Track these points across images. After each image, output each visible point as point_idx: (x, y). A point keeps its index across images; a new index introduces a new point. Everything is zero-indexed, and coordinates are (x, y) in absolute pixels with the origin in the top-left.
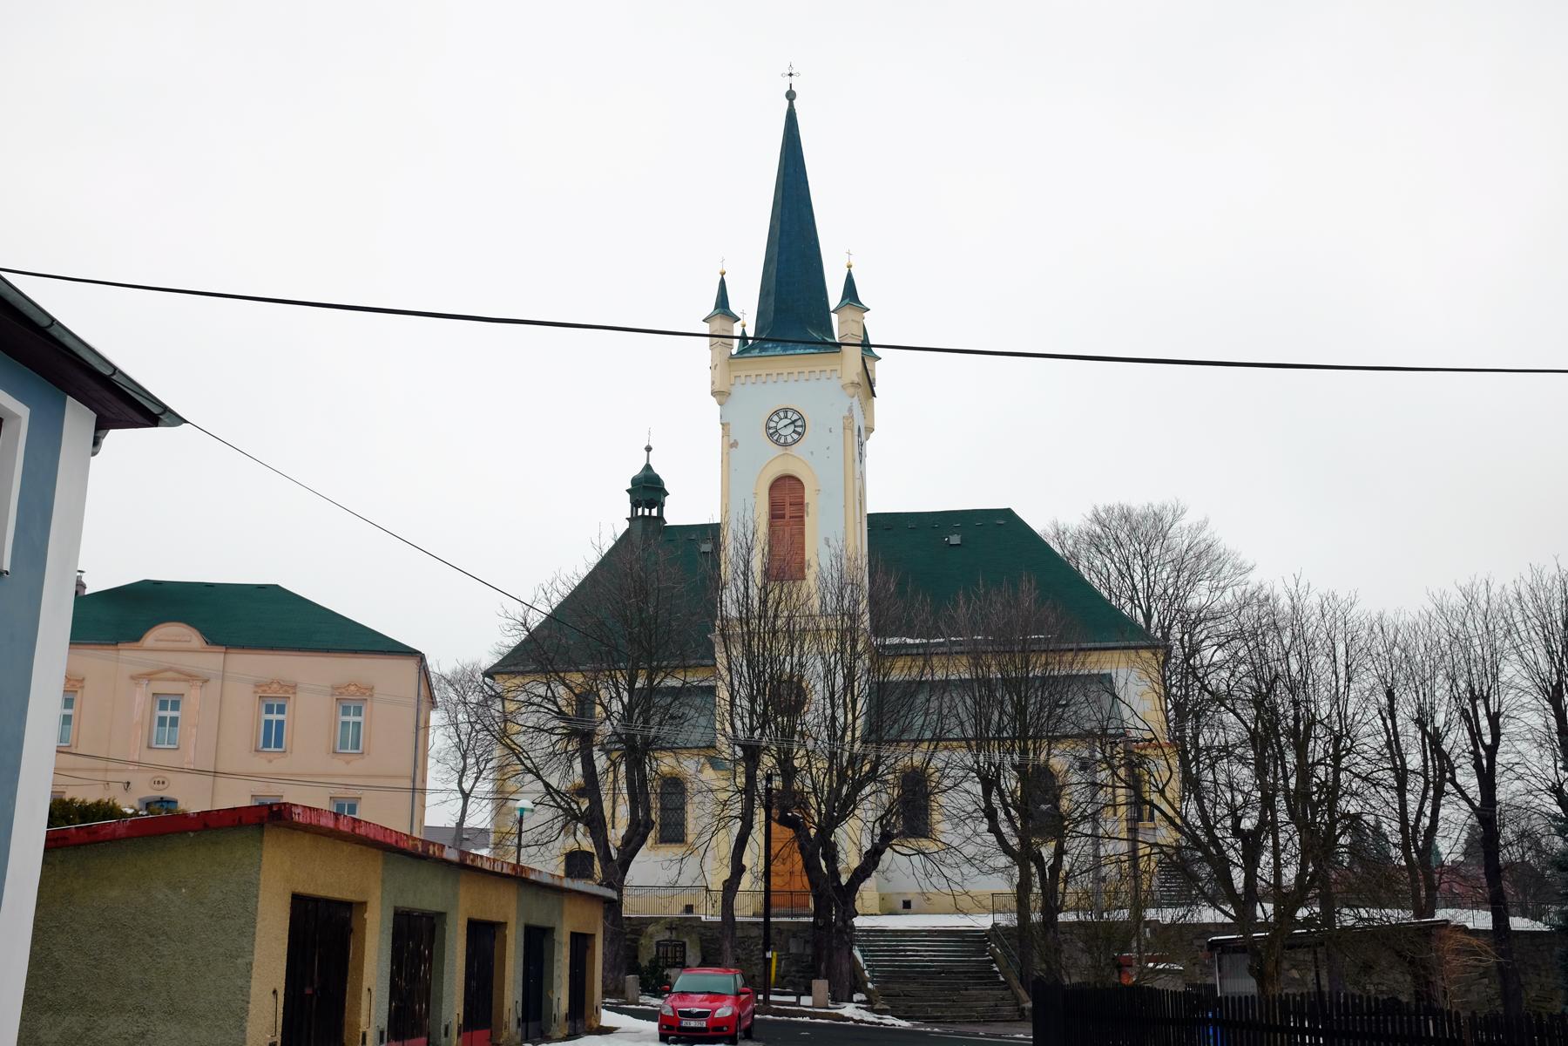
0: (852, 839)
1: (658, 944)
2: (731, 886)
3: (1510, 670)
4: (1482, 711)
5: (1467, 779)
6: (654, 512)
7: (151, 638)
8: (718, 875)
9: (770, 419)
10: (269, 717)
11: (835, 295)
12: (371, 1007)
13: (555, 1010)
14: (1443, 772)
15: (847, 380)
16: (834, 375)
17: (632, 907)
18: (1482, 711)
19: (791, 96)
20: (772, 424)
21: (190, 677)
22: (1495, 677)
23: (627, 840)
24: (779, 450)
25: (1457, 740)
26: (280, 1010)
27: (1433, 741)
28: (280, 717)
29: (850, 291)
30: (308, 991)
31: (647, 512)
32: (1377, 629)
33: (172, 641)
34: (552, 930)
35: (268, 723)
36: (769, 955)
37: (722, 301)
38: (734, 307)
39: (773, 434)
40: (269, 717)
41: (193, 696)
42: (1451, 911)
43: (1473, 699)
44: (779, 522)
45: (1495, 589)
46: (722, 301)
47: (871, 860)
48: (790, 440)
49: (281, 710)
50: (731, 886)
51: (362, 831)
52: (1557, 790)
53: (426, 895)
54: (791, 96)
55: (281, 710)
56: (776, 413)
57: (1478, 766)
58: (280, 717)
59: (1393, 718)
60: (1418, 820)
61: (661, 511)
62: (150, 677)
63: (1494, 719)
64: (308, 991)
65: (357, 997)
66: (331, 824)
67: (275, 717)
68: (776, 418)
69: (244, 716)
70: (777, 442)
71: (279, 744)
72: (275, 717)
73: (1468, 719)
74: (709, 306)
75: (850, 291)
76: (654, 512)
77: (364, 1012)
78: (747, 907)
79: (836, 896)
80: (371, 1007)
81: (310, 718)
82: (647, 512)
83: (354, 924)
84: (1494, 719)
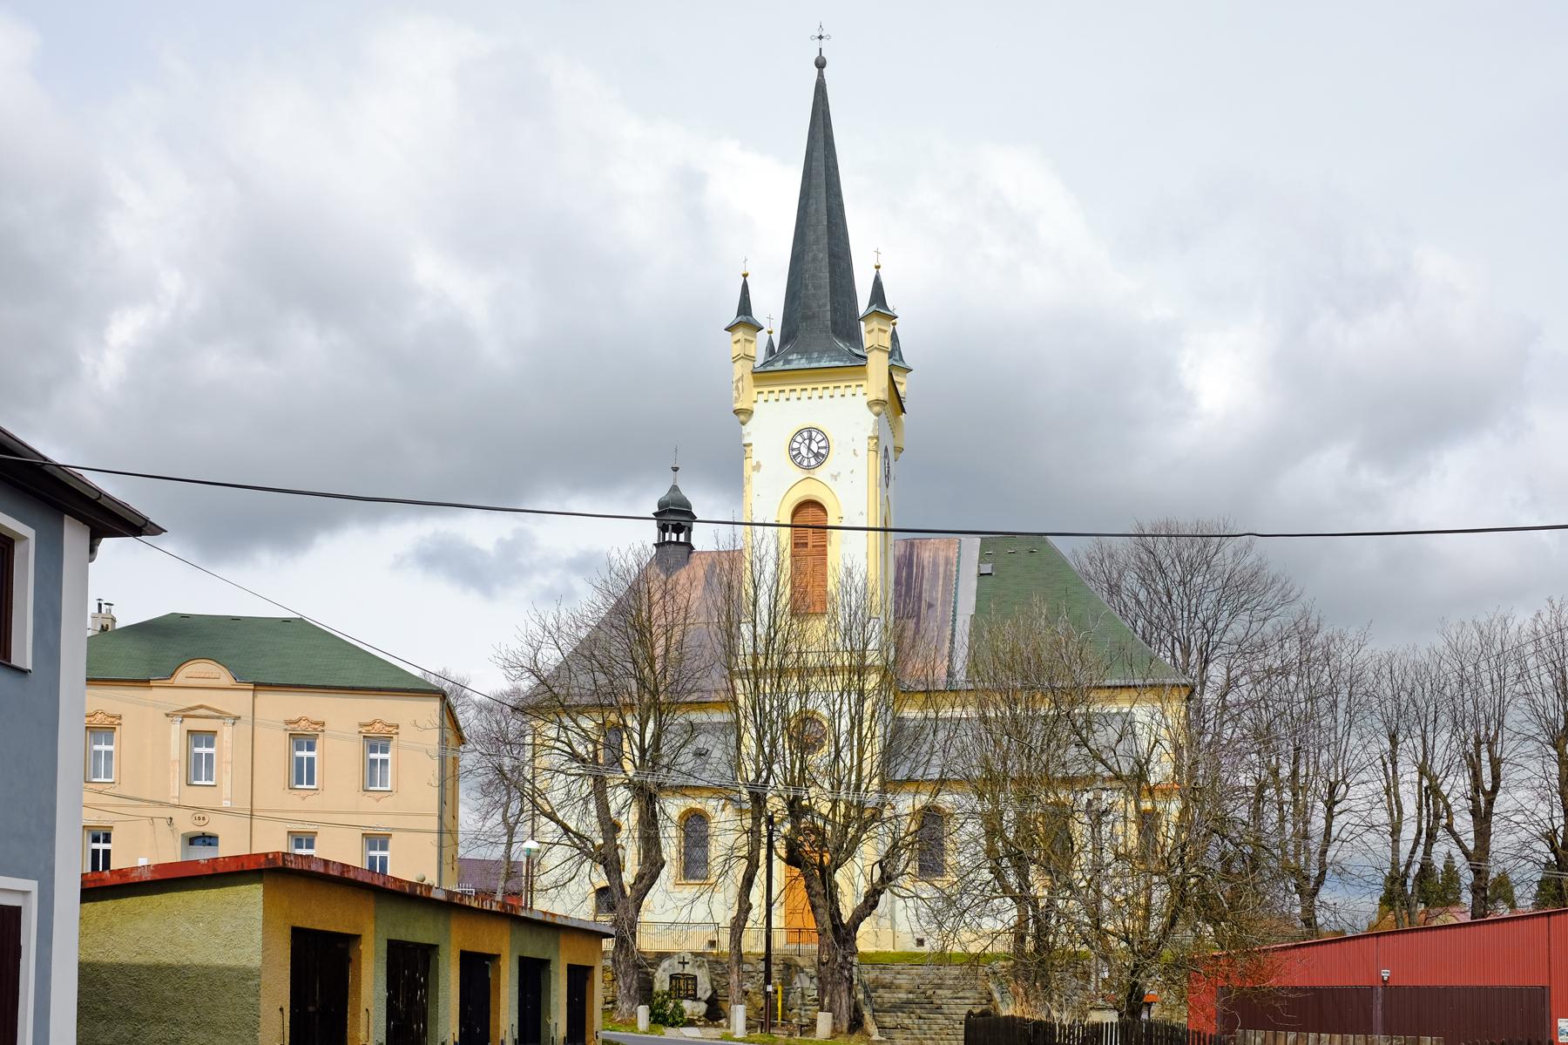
0: (851, 882)
1: (672, 977)
2: (738, 926)
3: (1516, 717)
4: (1485, 756)
5: (1464, 824)
6: (682, 538)
7: (181, 677)
8: (724, 913)
9: (793, 440)
10: (95, 846)
11: (863, 304)
12: (558, 1021)
13: (553, 1033)
14: (1437, 817)
15: (873, 397)
16: (860, 391)
17: (647, 942)
18: (1485, 756)
19: (820, 64)
20: (795, 445)
21: (220, 715)
22: (1500, 724)
23: (640, 877)
24: (800, 474)
25: (1456, 786)
26: (287, 1024)
27: (1431, 792)
28: (107, 846)
29: (878, 294)
30: (311, 1009)
31: (674, 537)
32: (1385, 671)
33: (203, 679)
34: (547, 962)
35: (95, 853)
36: (770, 988)
37: (745, 306)
38: (758, 314)
39: (795, 456)
40: (95, 846)
41: (226, 733)
42: (264, 1005)
43: (1478, 743)
44: (803, 551)
45: (1513, 629)
46: (745, 306)
47: (870, 904)
48: (819, 438)
49: (107, 840)
50: (738, 926)
51: (351, 875)
52: (1550, 837)
53: (419, 931)
54: (820, 64)
55: (107, 840)
57: (1474, 813)
58: (107, 846)
59: (1394, 764)
60: (1408, 866)
61: (688, 537)
62: (185, 714)
63: (1496, 763)
64: (311, 1009)
65: (357, 1015)
66: (321, 870)
67: (101, 846)
68: (799, 439)
69: (275, 752)
70: (800, 465)
71: (311, 781)
72: (101, 846)
73: (1474, 768)
74: (731, 315)
75: (878, 294)
76: (682, 538)
77: (363, 1028)
78: (753, 943)
79: (843, 934)
80: (558, 1021)
81: (338, 757)
82: (674, 536)
83: (352, 955)
84: (1496, 763)
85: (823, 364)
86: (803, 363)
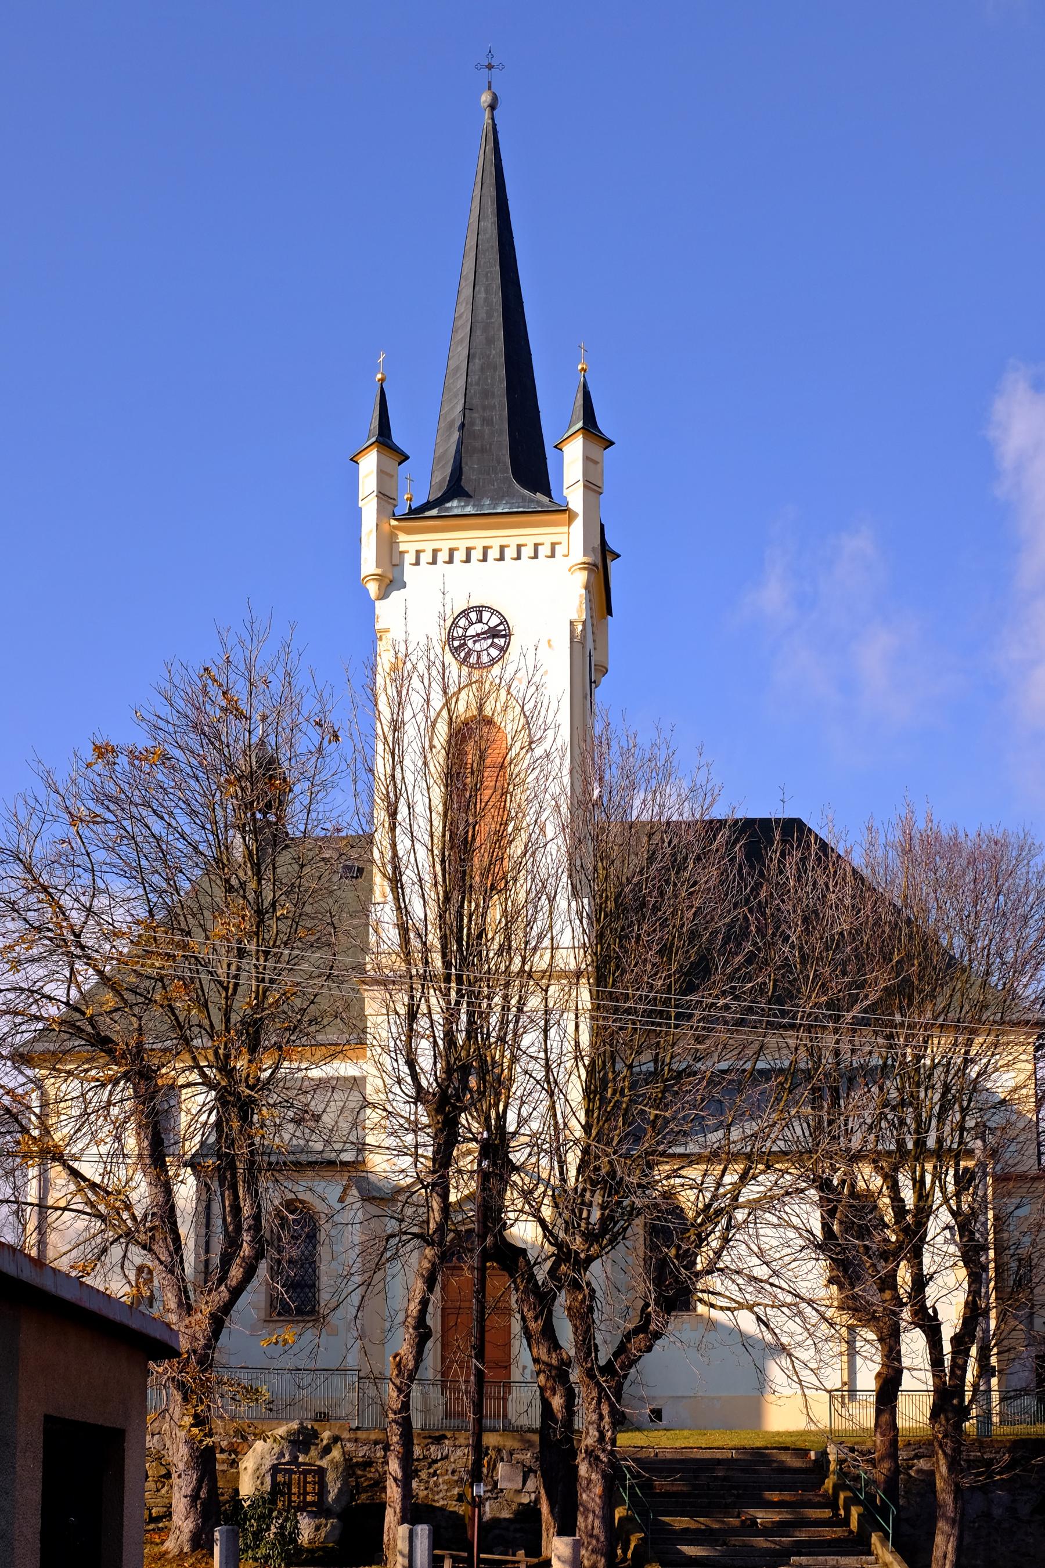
56: (465, 613)
68: (463, 622)
85: (499, 511)
86: (469, 510)
